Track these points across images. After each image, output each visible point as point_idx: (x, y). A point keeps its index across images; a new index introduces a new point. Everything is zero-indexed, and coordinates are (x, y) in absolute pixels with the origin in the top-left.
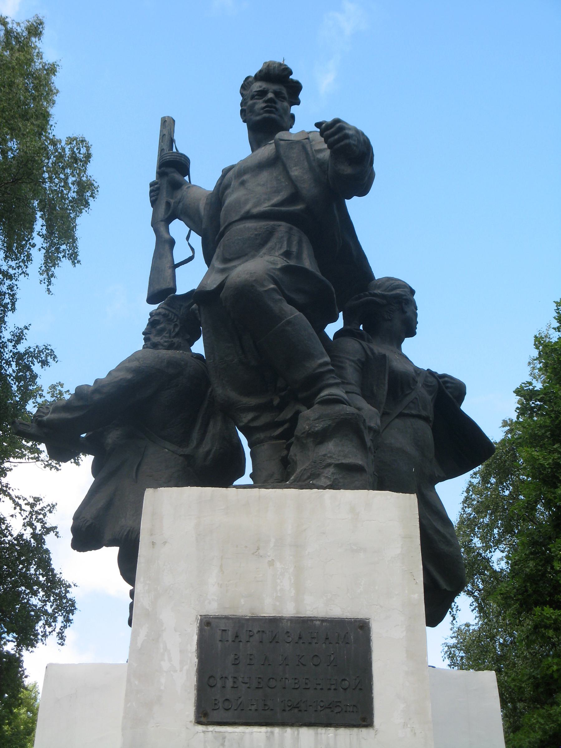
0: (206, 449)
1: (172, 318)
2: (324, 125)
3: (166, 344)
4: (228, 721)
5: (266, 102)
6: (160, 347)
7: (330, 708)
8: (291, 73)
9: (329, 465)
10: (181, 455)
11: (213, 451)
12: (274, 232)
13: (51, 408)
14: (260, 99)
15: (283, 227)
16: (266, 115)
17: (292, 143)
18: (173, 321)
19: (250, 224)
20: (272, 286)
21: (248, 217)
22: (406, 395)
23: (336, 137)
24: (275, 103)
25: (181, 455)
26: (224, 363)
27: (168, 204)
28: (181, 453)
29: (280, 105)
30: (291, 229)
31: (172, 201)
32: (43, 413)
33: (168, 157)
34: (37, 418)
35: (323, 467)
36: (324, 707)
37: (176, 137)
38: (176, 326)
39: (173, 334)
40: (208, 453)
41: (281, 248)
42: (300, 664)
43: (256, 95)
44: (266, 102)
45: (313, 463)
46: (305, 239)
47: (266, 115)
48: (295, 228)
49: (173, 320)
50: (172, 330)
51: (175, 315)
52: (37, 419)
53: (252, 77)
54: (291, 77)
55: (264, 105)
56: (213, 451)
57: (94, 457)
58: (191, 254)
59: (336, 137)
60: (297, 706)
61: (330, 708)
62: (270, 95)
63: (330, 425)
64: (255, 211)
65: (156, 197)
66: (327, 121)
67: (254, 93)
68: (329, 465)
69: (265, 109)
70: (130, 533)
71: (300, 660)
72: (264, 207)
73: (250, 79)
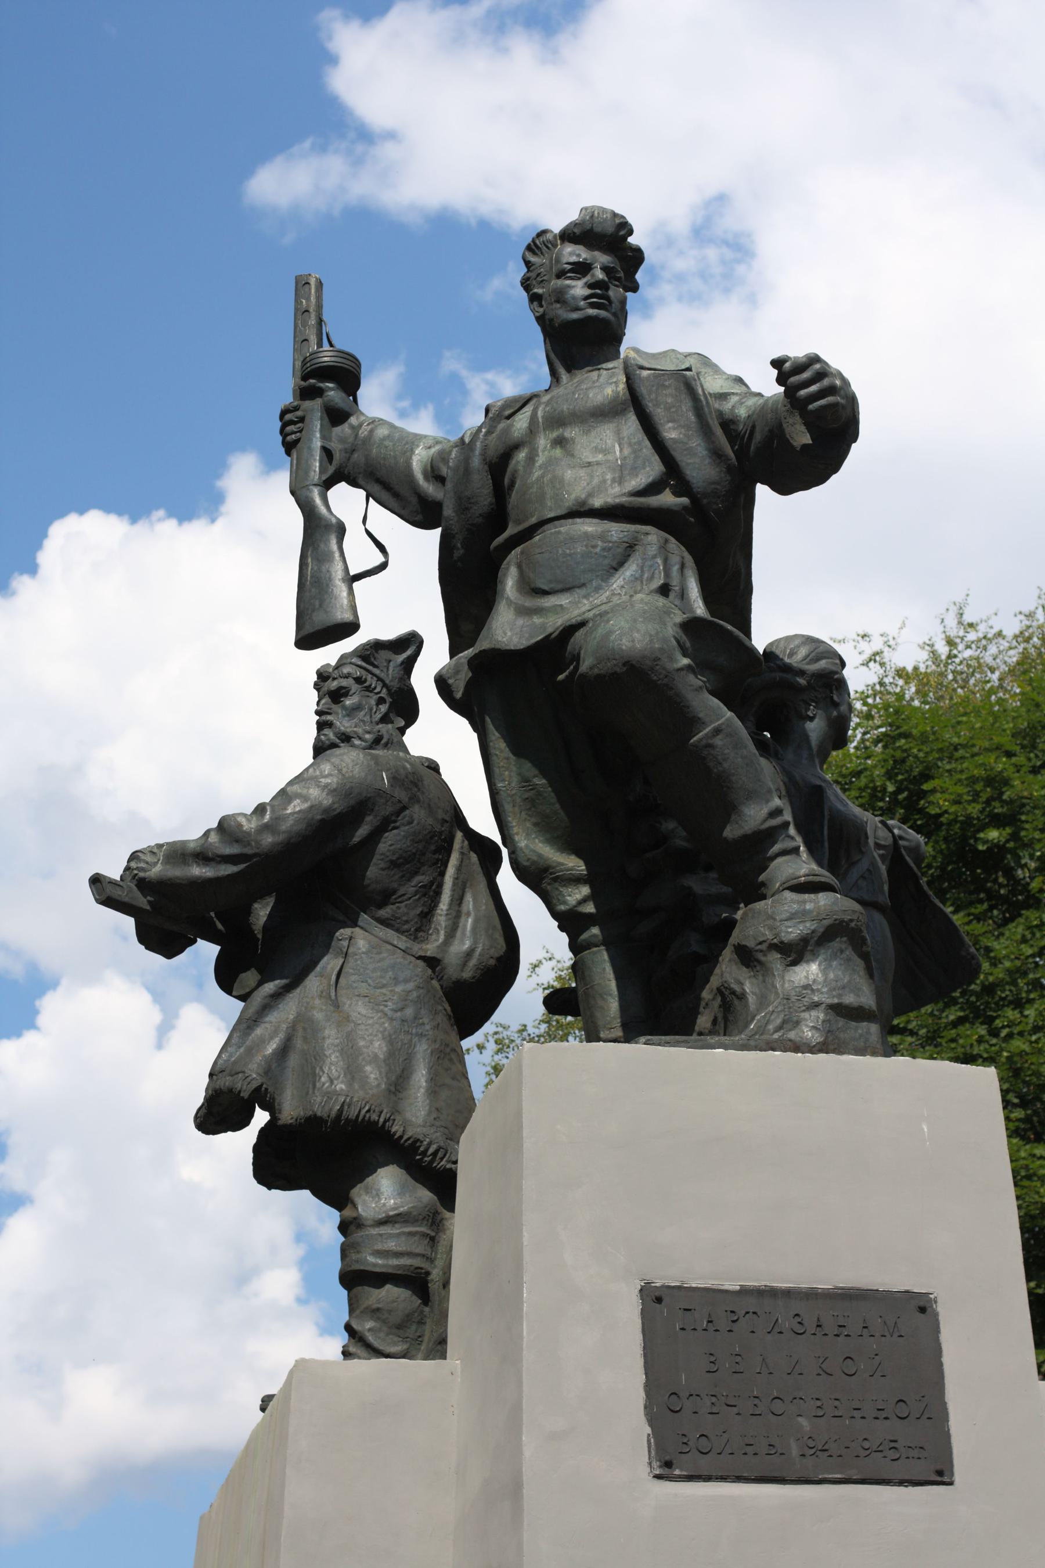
0: (467, 944)
1: (373, 686)
2: (787, 365)
3: (367, 736)
4: (776, 1475)
5: (590, 286)
6: (357, 742)
7: (881, 1451)
8: (631, 232)
9: (816, 1005)
10: (420, 958)
11: (479, 950)
12: (635, 545)
13: (162, 854)
14: (579, 279)
15: (652, 537)
16: (592, 312)
17: (663, 375)
18: (376, 691)
19: (589, 526)
20: (686, 661)
21: (582, 511)
22: (853, 864)
23: (814, 388)
24: (607, 289)
25: (420, 958)
26: (531, 790)
27: (327, 453)
28: (419, 954)
29: (614, 292)
30: (666, 541)
31: (335, 446)
32: (147, 863)
33: (326, 359)
34: (136, 872)
35: (804, 1008)
36: (870, 1451)
37: (324, 318)
38: (381, 701)
39: (378, 716)
40: (469, 954)
41: (651, 578)
42: (821, 1372)
43: (570, 271)
44: (590, 286)
45: (785, 1001)
46: (689, 559)
47: (592, 312)
48: (672, 540)
49: (375, 688)
50: (375, 710)
51: (379, 679)
52: (136, 874)
53: (552, 232)
54: (630, 240)
55: (587, 292)
56: (479, 950)
57: (219, 948)
58: (382, 559)
59: (814, 388)
60: (879, 1449)
61: (881, 1451)
62: (600, 275)
63: (813, 932)
64: (597, 502)
65: (298, 434)
66: (791, 355)
67: (566, 266)
68: (816, 1005)
69: (589, 301)
70: (346, 1107)
71: (822, 1366)
72: (612, 494)
73: (549, 236)
